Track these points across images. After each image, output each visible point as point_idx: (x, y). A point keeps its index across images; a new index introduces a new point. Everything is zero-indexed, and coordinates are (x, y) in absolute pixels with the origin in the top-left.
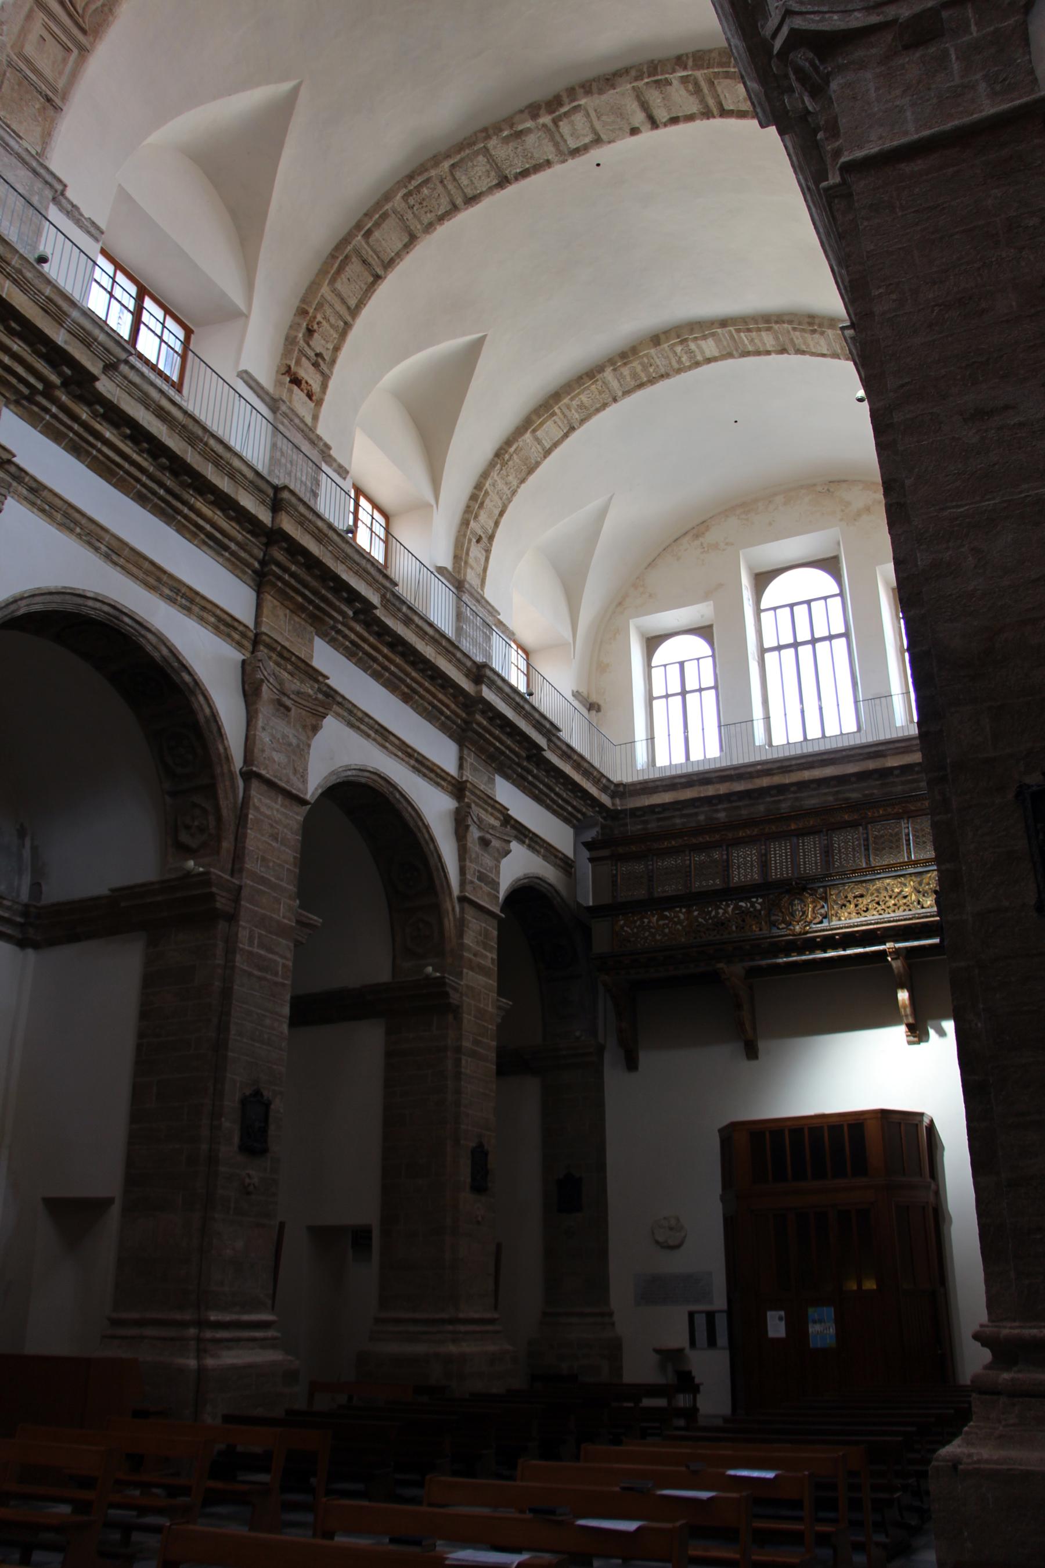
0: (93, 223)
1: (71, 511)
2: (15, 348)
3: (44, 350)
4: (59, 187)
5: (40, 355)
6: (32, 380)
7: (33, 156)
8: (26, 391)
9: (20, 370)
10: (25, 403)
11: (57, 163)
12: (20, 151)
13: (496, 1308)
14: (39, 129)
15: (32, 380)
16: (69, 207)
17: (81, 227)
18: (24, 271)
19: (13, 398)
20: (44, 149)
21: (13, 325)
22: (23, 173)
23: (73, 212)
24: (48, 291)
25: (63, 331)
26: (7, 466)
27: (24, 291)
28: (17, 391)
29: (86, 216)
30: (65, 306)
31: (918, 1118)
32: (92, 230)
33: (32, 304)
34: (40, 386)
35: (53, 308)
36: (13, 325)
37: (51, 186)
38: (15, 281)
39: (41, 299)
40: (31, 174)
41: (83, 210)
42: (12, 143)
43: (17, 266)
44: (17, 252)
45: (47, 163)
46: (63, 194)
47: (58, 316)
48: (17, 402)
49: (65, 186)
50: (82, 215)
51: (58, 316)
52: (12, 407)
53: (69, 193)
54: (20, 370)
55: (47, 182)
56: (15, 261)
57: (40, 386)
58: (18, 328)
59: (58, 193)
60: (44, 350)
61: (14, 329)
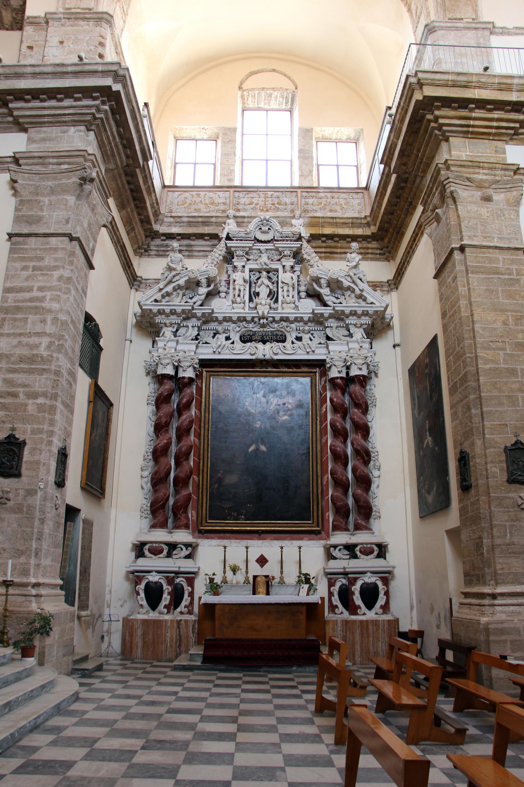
0: (516, 28)
1: (355, 221)
2: (496, 116)
3: (510, 108)
4: (490, 26)
5: (510, 111)
6: (512, 125)
7: (471, 23)
8: (512, 132)
9: (504, 124)
10: (515, 137)
11: (485, 16)
12: (464, 25)
13: (254, 593)
14: (470, 8)
15: (512, 125)
16: (501, 31)
17: (511, 35)
18: (481, 80)
19: (508, 139)
20: (477, 15)
21: (489, 107)
22: (471, 34)
23: (504, 32)
24: (497, 80)
25: (514, 93)
26: (518, 172)
27: (486, 89)
28: (508, 135)
29: (511, 27)
30: (509, 81)
31: (423, 515)
32: (518, 31)
33: (492, 91)
34: (517, 125)
35: (503, 86)
36: (489, 107)
37: (486, 28)
38: (479, 87)
39: (496, 86)
40: (475, 31)
41: (508, 27)
42: (459, 25)
43: (476, 80)
44: (473, 74)
45: (481, 20)
46: (494, 27)
47: (508, 88)
48: (511, 139)
49: (493, 23)
50: (509, 29)
51: (508, 88)
52: (510, 143)
53: (497, 25)
54: (504, 124)
55: (483, 29)
56: (474, 79)
57: (517, 125)
58: (492, 107)
59: (492, 29)
60: (510, 108)
61: (490, 108)
